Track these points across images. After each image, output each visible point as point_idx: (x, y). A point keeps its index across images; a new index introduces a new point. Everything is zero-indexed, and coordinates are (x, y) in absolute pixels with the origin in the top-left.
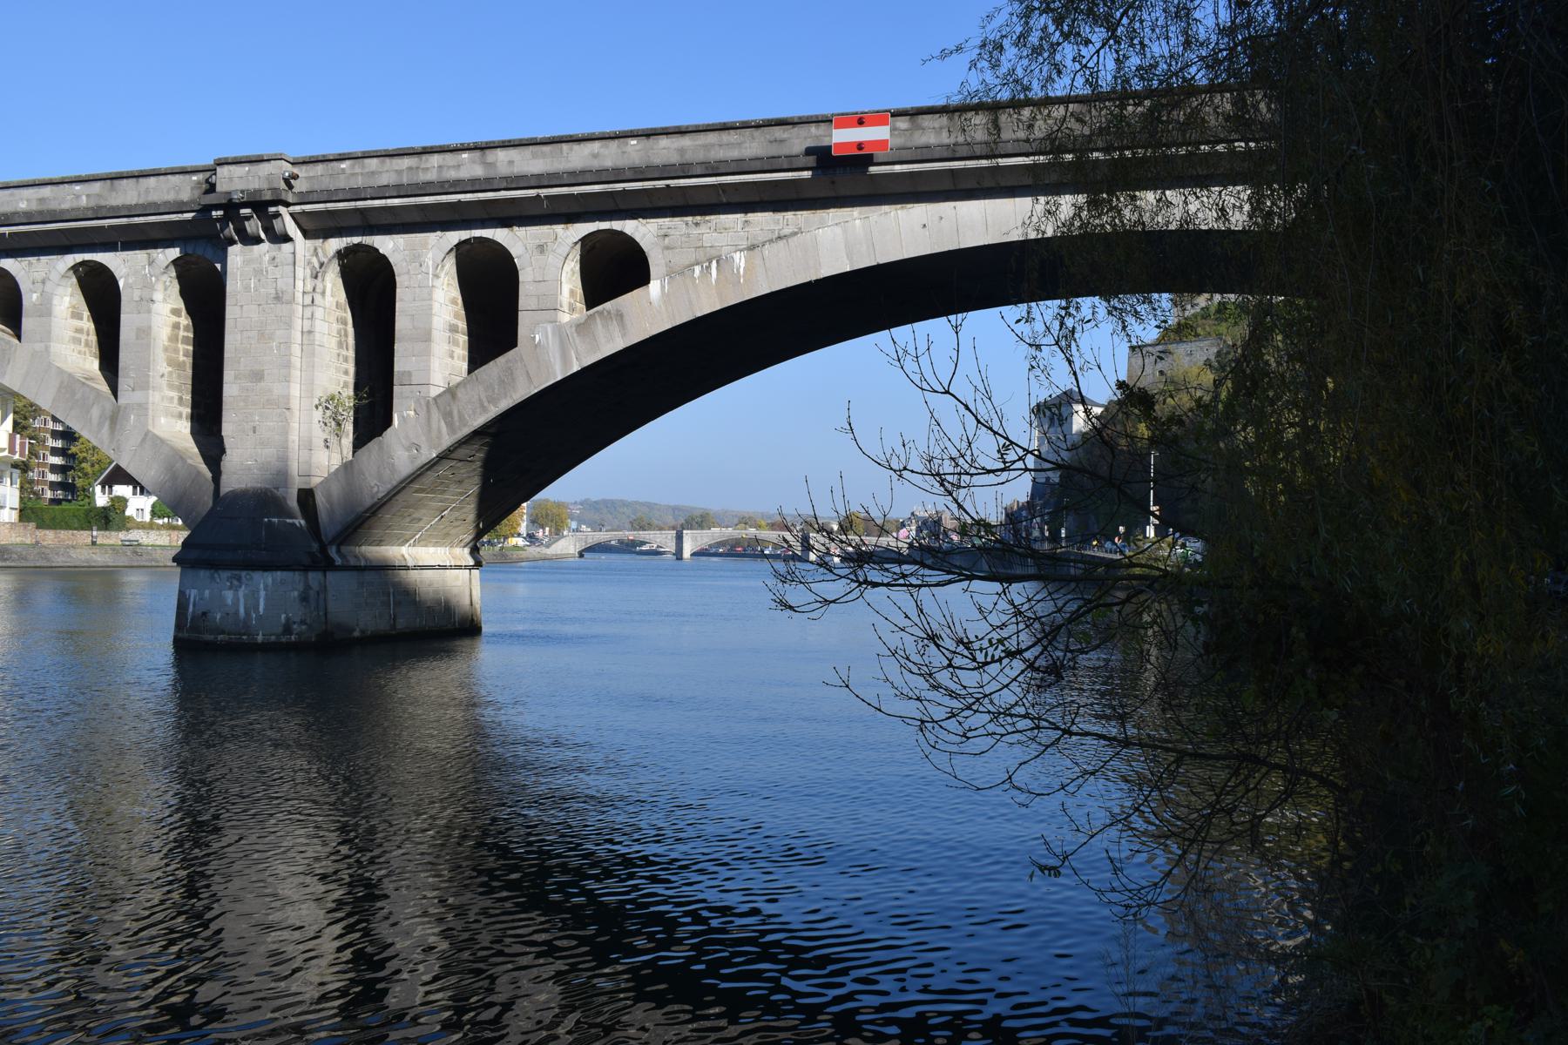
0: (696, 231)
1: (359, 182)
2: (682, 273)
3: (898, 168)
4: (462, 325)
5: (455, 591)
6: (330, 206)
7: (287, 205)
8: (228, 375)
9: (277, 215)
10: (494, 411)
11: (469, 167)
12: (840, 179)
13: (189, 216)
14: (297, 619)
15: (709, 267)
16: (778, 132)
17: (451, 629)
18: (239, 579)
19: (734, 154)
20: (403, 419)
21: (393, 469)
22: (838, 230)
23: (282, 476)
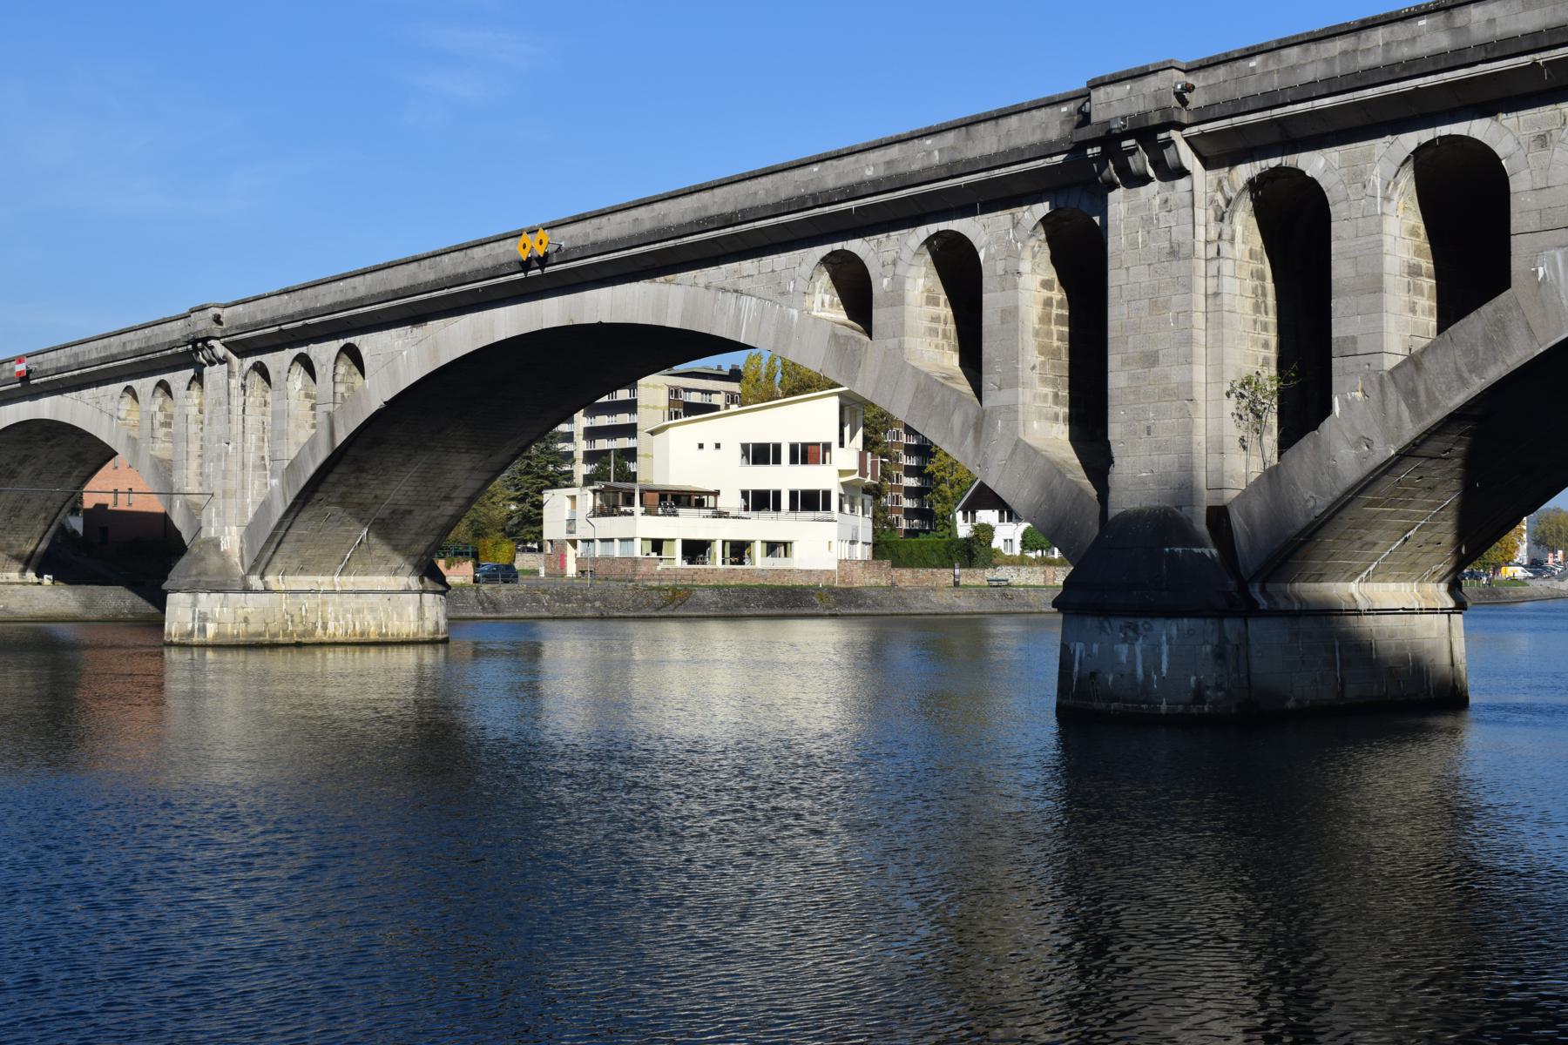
1: (1275, 83)
6: (1237, 121)
7: (1181, 127)
8: (1114, 361)
9: (1169, 142)
13: (1059, 159)
14: (1211, 683)
17: (1422, 700)
18: (1135, 629)
20: (1347, 404)
21: (1335, 474)
23: (1186, 490)
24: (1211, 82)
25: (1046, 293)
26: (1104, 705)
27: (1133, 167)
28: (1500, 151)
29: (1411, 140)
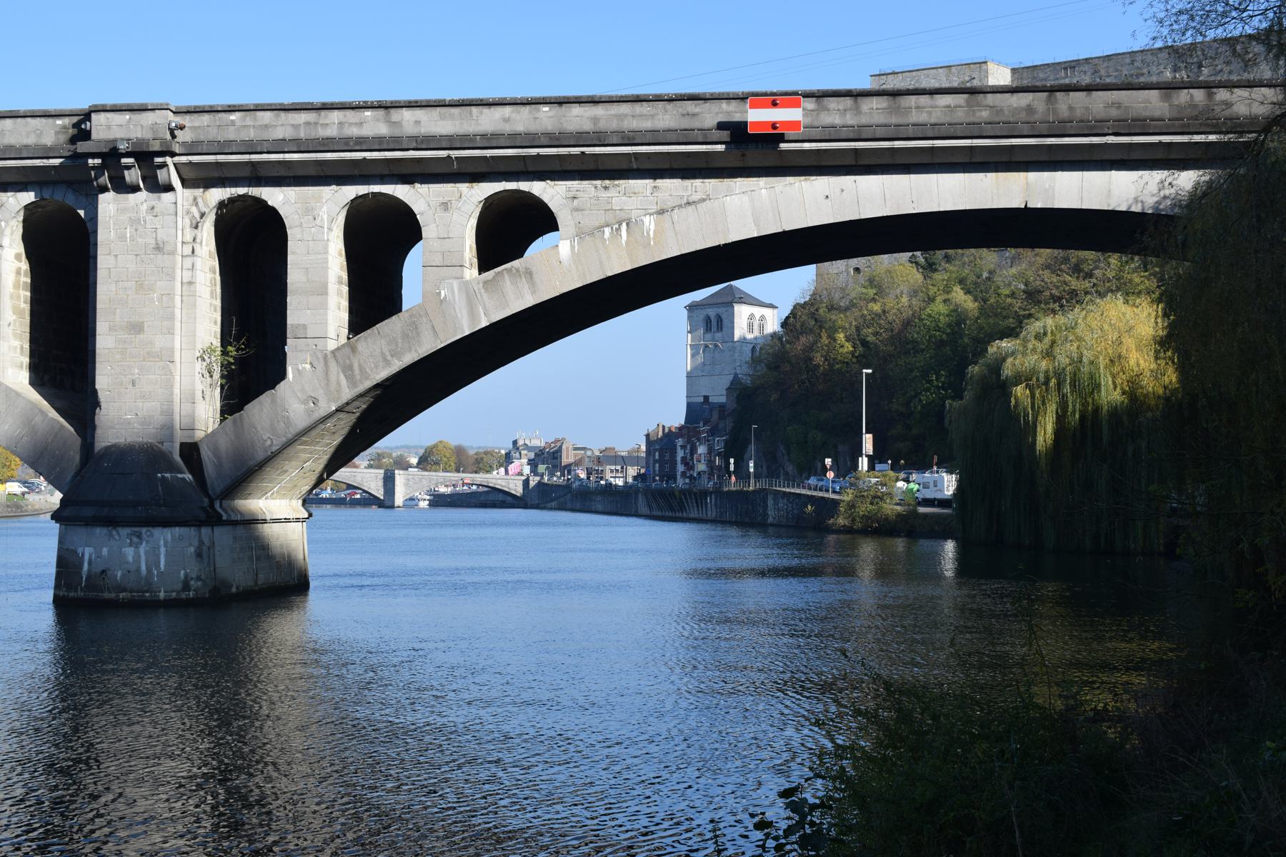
0: (605, 194)
1: (251, 134)
2: (591, 234)
3: (807, 146)
4: (345, 276)
5: (294, 545)
6: (221, 158)
7: (173, 154)
8: (102, 327)
9: (164, 165)
10: (397, 366)
11: (372, 125)
12: (752, 152)
13: (57, 162)
14: (194, 575)
15: (619, 229)
16: (690, 106)
17: (289, 585)
18: (139, 536)
19: (647, 125)
20: (299, 372)
21: (288, 422)
22: (745, 198)
23: (169, 428)
24: (196, 124)
25: (17, 264)
26: (113, 595)
27: (128, 178)
28: (416, 209)
29: (352, 192)
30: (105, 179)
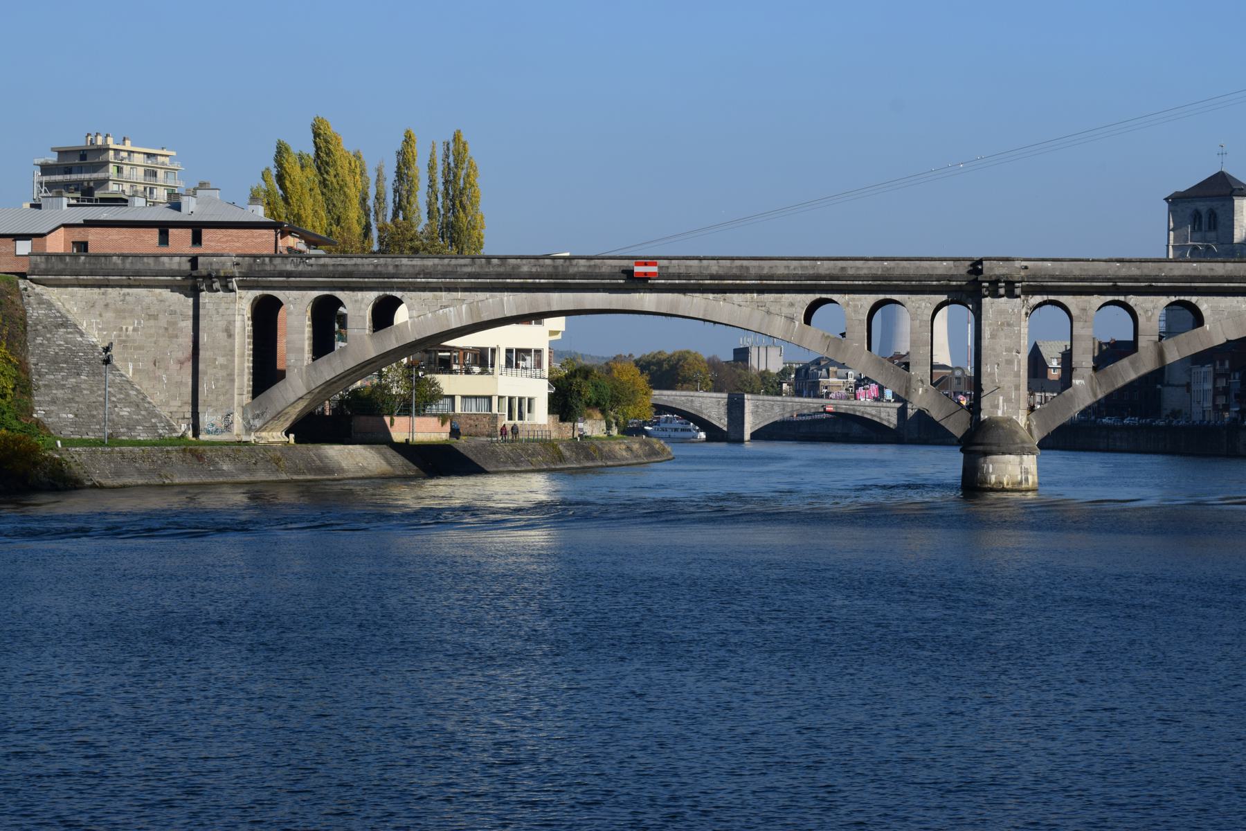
29: (258, 293)
30: (204, 287)
